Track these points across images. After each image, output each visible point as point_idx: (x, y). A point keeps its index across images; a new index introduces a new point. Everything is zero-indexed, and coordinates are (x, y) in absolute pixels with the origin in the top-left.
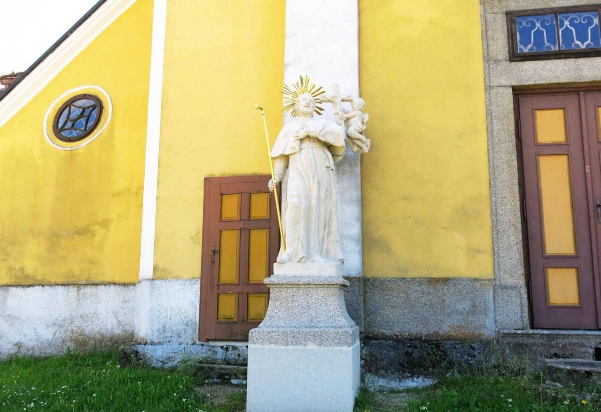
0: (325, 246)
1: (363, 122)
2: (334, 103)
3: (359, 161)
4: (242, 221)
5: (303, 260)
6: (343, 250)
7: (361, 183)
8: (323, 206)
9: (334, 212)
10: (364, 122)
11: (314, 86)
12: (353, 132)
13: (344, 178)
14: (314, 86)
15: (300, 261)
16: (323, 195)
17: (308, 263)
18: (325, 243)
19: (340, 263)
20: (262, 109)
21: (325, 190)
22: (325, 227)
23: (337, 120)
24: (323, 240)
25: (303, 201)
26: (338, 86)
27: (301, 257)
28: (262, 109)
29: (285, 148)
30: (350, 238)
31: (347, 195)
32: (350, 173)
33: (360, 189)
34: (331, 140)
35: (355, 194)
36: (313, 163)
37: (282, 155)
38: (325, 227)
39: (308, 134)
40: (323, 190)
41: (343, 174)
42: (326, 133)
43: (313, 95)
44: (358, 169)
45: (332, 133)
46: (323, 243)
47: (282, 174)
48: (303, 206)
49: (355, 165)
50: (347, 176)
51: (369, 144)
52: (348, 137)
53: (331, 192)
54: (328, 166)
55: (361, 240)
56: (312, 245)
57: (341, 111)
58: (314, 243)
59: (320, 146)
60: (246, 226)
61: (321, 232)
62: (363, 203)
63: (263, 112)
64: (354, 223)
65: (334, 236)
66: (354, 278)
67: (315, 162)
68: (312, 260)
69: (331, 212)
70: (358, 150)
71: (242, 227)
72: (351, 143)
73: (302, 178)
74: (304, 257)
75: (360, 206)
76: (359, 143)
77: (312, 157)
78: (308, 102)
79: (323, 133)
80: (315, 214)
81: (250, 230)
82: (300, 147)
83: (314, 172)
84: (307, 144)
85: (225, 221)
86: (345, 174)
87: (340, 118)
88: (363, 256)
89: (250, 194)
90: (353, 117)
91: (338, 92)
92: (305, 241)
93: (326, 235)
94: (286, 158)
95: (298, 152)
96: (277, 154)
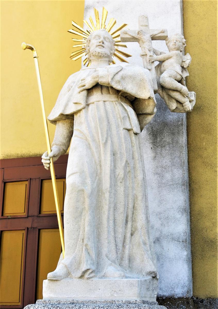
0: (127, 252)
1: (183, 67)
2: (141, 41)
3: (185, 128)
4: (30, 219)
5: (86, 276)
6: (159, 258)
7: (188, 159)
8: (121, 189)
9: (140, 198)
10: (185, 67)
11: (115, 22)
12: (168, 79)
13: (163, 152)
14: (115, 22)
15: (82, 277)
16: (120, 172)
17: (95, 279)
18: (127, 247)
19: (150, 277)
20: (32, 49)
21: (123, 164)
22: (127, 221)
23: (145, 63)
24: (124, 242)
25: (89, 181)
26: (147, 18)
27: (84, 269)
28: (32, 49)
29: (66, 105)
30: (173, 239)
31: (168, 176)
32: (171, 145)
33: (186, 167)
34: (131, 89)
35: (179, 174)
36: (105, 123)
37: (62, 115)
38: (127, 221)
39: (96, 80)
40: (121, 165)
41: (163, 147)
42: (123, 78)
43: (114, 36)
44: (183, 139)
45: (132, 78)
46: (124, 246)
47: (64, 144)
48: (88, 189)
49: (178, 133)
50: (168, 148)
51: (193, 98)
52: (162, 87)
53: (134, 168)
54: (129, 127)
55: (189, 240)
56: (105, 251)
57: (150, 51)
58: (108, 248)
59: (116, 99)
60: (35, 225)
61: (120, 230)
62: (192, 187)
63: (35, 53)
64: (178, 216)
65: (140, 236)
66: (180, 298)
67: (109, 123)
68: (102, 274)
69: (135, 199)
70: (177, 108)
71: (29, 226)
72: (166, 97)
73: (89, 147)
74: (88, 270)
75: (187, 191)
76: (176, 95)
77: (103, 115)
78: (102, 39)
79: (118, 77)
80: (107, 202)
81: (39, 230)
82: (87, 102)
83: (105, 136)
84: (97, 96)
85: (7, 218)
86: (164, 146)
87: (148, 60)
88: (193, 265)
89: (42, 180)
90: (167, 59)
91: (147, 26)
92: (91, 244)
93: (128, 235)
94: (70, 118)
95: (84, 108)
96: (55, 115)
